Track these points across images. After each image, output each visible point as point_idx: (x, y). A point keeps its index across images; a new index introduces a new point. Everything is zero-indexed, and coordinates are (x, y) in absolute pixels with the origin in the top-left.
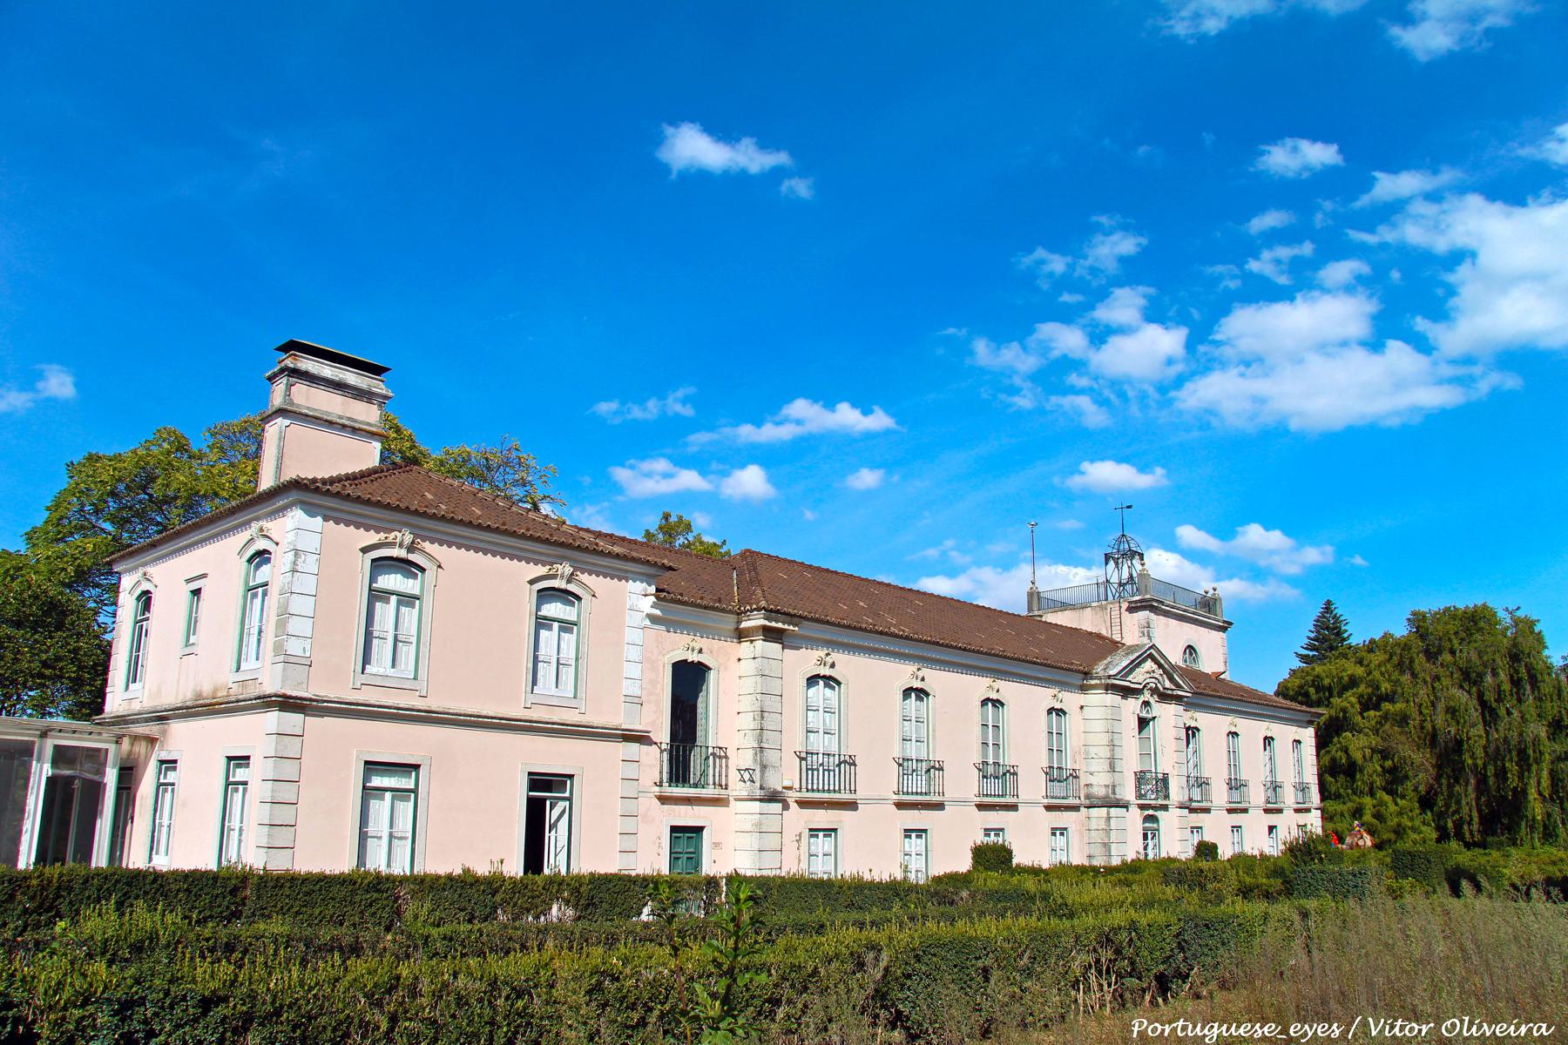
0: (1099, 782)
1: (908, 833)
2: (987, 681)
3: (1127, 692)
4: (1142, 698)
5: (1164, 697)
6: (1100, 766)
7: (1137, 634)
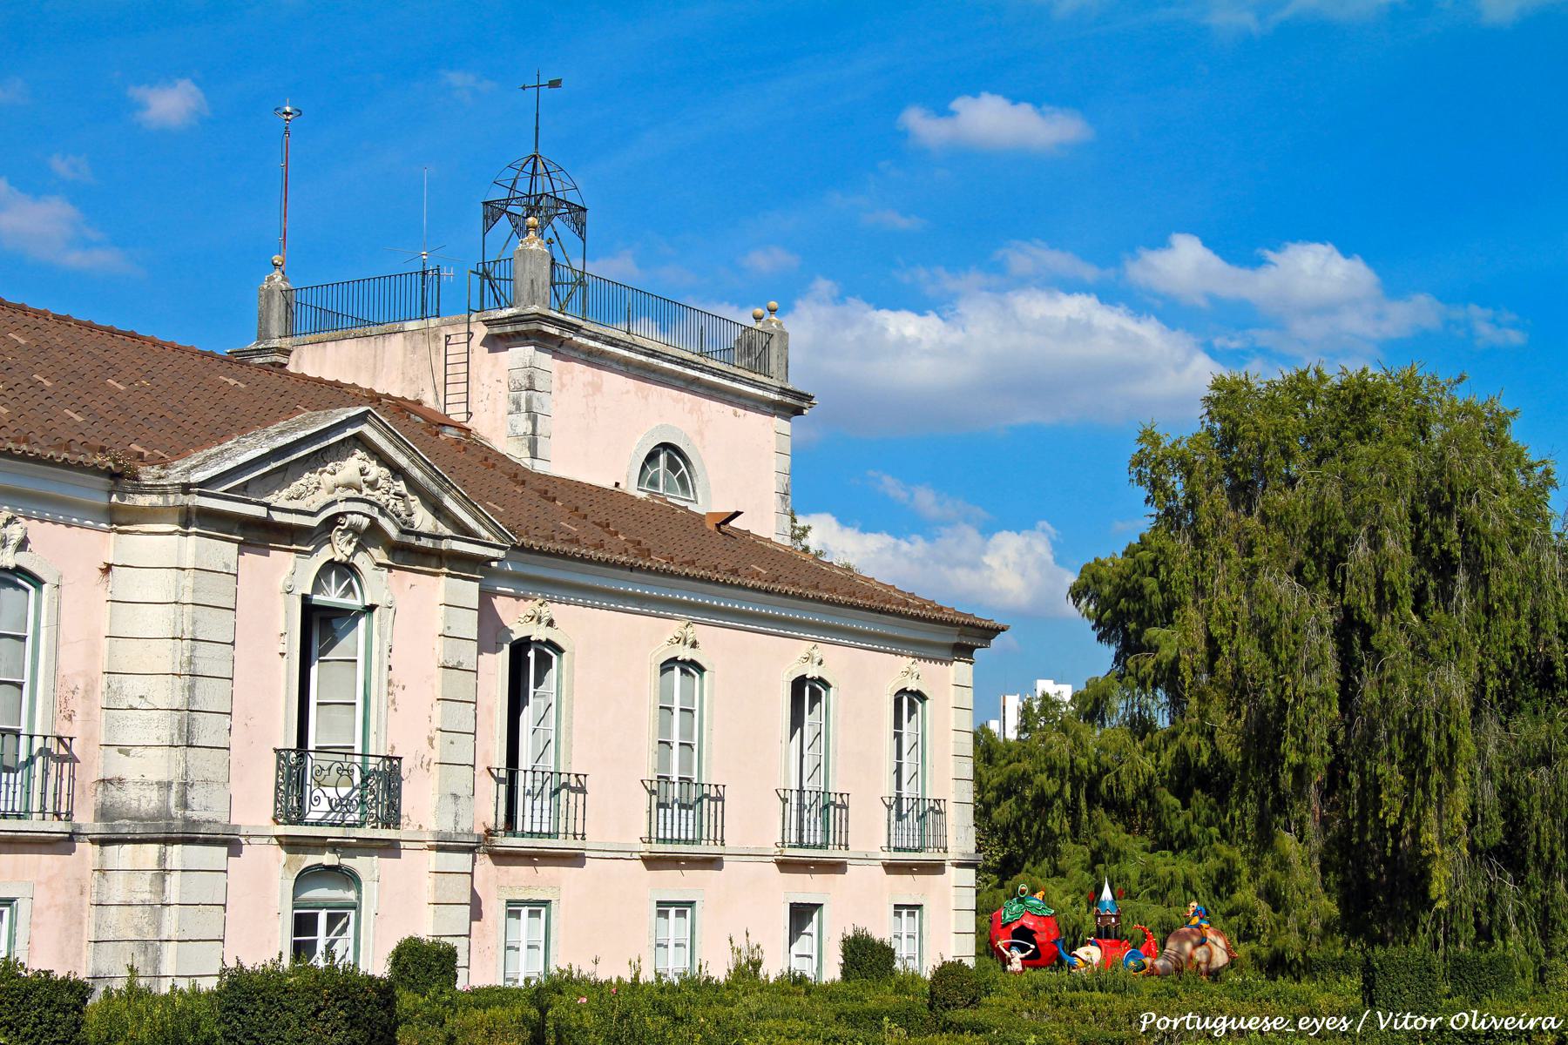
0: (144, 778)
1: (663, 907)
2: (905, 662)
3: (261, 535)
4: (325, 554)
5: (409, 554)
6: (155, 728)
7: (504, 405)
